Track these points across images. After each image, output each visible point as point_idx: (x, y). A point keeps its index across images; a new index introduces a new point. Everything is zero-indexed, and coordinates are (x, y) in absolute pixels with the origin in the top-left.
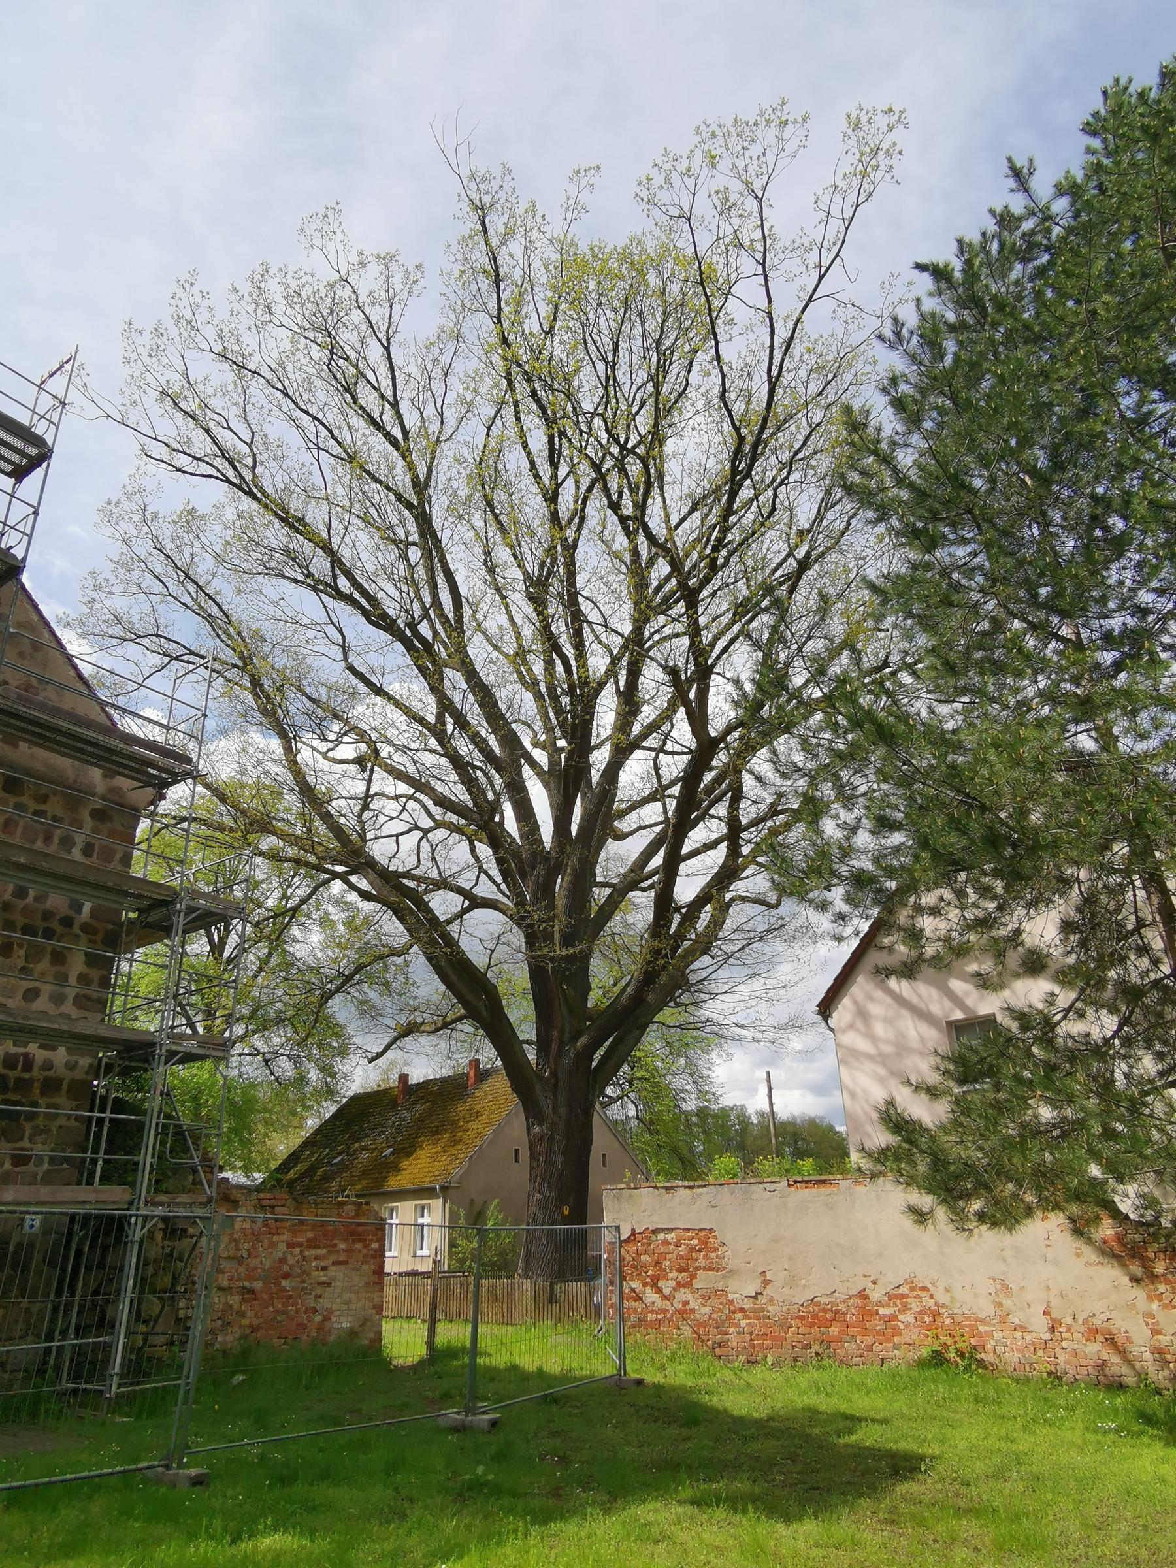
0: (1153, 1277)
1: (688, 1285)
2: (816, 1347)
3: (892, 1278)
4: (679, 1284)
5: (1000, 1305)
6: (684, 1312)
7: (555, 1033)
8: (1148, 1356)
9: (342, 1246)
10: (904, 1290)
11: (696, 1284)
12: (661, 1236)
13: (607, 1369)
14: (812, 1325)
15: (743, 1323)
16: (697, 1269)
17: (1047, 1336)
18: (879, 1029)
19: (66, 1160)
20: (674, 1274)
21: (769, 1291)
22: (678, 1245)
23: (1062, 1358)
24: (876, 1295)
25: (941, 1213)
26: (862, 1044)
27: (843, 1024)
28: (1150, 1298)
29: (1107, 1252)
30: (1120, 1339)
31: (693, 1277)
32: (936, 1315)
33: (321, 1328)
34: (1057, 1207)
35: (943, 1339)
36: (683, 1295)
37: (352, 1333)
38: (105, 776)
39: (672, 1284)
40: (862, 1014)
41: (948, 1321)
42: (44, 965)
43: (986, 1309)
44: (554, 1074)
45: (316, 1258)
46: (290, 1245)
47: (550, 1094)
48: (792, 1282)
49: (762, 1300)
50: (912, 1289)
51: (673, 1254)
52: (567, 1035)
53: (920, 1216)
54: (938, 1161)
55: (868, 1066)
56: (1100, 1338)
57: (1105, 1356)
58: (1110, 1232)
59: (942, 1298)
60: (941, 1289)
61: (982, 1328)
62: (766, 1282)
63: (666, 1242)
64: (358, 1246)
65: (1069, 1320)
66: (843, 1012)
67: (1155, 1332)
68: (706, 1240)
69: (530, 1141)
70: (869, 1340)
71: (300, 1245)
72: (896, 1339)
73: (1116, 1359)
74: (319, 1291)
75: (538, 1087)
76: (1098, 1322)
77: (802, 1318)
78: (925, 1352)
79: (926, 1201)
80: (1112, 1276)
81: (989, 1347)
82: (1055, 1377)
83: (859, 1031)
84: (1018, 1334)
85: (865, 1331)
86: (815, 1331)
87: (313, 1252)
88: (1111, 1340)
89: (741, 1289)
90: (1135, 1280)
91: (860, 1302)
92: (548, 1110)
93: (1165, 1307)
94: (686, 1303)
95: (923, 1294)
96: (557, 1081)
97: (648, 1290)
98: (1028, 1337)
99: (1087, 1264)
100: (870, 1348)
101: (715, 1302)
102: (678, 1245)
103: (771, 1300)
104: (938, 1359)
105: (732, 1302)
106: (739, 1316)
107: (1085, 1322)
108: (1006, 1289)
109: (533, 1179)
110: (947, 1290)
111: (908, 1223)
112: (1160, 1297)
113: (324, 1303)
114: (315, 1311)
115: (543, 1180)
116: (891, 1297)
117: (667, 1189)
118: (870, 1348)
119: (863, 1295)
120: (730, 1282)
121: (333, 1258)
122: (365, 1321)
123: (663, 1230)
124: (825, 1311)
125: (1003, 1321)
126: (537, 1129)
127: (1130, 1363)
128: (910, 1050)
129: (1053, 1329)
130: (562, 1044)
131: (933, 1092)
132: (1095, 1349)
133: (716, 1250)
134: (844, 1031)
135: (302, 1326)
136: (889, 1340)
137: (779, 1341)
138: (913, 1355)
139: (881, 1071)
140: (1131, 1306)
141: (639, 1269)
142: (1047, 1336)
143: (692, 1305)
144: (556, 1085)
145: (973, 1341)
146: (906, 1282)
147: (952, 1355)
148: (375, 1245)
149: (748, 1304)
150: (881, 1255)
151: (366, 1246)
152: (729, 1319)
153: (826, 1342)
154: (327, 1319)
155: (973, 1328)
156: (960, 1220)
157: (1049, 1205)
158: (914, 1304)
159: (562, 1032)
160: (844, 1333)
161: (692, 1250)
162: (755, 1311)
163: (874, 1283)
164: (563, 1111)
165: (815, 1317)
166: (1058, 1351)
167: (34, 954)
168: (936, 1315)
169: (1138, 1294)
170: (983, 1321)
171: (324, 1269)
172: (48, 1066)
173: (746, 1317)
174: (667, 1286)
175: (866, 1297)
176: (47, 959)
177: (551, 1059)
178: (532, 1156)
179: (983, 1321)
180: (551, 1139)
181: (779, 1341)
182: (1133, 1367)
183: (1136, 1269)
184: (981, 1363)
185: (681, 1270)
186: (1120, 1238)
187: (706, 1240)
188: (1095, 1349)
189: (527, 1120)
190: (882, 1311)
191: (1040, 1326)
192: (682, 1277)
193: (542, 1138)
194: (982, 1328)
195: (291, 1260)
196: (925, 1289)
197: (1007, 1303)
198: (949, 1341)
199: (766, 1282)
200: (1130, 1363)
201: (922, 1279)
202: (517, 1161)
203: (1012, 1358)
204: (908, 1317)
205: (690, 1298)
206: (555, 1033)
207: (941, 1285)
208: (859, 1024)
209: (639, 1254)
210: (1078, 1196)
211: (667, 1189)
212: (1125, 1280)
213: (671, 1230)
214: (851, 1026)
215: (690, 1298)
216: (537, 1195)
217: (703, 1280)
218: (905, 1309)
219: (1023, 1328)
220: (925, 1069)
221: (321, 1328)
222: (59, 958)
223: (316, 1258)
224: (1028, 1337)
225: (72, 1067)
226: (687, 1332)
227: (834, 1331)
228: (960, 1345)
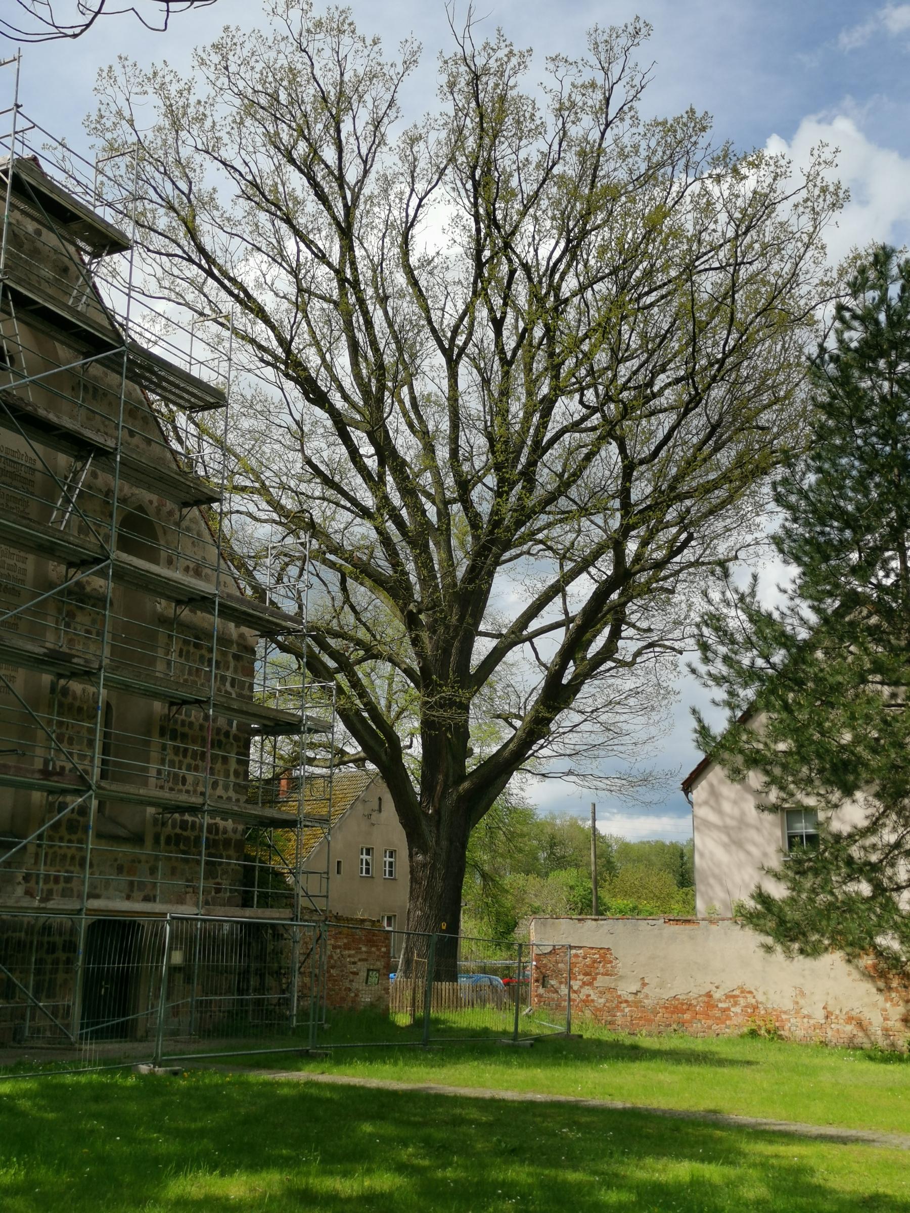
0: (890, 989)
1: (590, 984)
2: (674, 1026)
3: (730, 983)
4: (584, 984)
5: (797, 1003)
6: (587, 1001)
7: (441, 777)
8: (879, 1032)
9: (364, 949)
10: (737, 993)
11: (596, 984)
12: (573, 952)
13: (560, 1028)
14: (673, 1013)
15: (627, 1010)
16: (598, 974)
17: (823, 1021)
18: (727, 807)
19: (236, 890)
20: (581, 977)
21: (646, 990)
22: (585, 958)
23: (830, 1033)
24: (717, 995)
25: (779, 948)
26: (712, 817)
27: (700, 801)
28: (886, 1000)
29: (867, 975)
30: (865, 1023)
31: (594, 979)
32: (755, 1008)
33: (353, 1001)
34: (841, 948)
35: (758, 1022)
36: (587, 990)
37: (372, 1005)
38: (236, 626)
39: (579, 983)
40: (714, 792)
41: (763, 1012)
42: (219, 766)
43: (788, 1005)
44: (437, 812)
45: (349, 956)
46: (335, 947)
47: (434, 829)
48: (661, 985)
49: (640, 996)
50: (742, 992)
51: (581, 964)
52: (451, 779)
53: (769, 949)
54: (782, 922)
55: (716, 834)
56: (854, 1022)
57: (855, 1032)
58: (870, 962)
59: (761, 998)
60: (761, 992)
61: (784, 1017)
62: (644, 985)
63: (576, 956)
64: (373, 949)
65: (837, 1012)
66: (699, 792)
67: (886, 1019)
68: (605, 955)
69: (411, 867)
70: (710, 1022)
71: (339, 947)
72: (728, 1022)
73: (861, 1034)
74: (351, 976)
75: (424, 822)
76: (854, 1013)
77: (666, 1008)
78: (745, 1030)
79: (770, 940)
80: (868, 987)
81: (786, 1027)
82: (824, 1044)
83: (712, 807)
84: (806, 1020)
85: (708, 1017)
86: (675, 1016)
87: (346, 952)
88: (860, 1024)
89: (626, 989)
90: (880, 990)
91: (706, 999)
92: (432, 842)
93: (894, 1005)
94: (588, 996)
95: (748, 995)
96: (440, 818)
97: (563, 986)
98: (812, 1022)
99: (854, 980)
100: (710, 1027)
101: (608, 996)
102: (585, 958)
103: (647, 996)
104: (754, 1034)
105: (620, 996)
106: (624, 1005)
107: (847, 1013)
108: (802, 994)
109: (413, 896)
110: (764, 993)
111: (761, 952)
112: (892, 1000)
113: (355, 985)
114: (350, 990)
115: (425, 900)
116: (728, 997)
117: (579, 920)
118: (710, 1027)
119: (709, 995)
120: (619, 983)
121: (359, 957)
122: (380, 998)
123: (575, 947)
124: (682, 1004)
125: (797, 1012)
126: (420, 857)
127: (868, 1036)
128: (748, 825)
129: (827, 1017)
130: (446, 787)
131: (777, 877)
132: (850, 1028)
133: (611, 962)
134: (700, 805)
135: (343, 999)
136: (724, 1023)
137: (650, 1021)
138: (737, 1032)
139: (725, 839)
140: (875, 1005)
141: (558, 973)
142: (823, 1021)
143: (592, 997)
144: (439, 822)
145: (777, 1024)
146: (738, 988)
147: (763, 1032)
148: (383, 949)
149: (631, 998)
150: (724, 971)
151: (379, 950)
152: (617, 1007)
153: (681, 1023)
154: (356, 995)
155: (778, 1016)
156: (788, 952)
157: (836, 944)
158: (742, 1002)
159: (446, 776)
160: (694, 1018)
161: (594, 961)
162: (635, 1002)
163: (717, 987)
164: (444, 843)
165: (675, 1007)
166: (829, 1030)
167: (214, 758)
168: (755, 1008)
169: (880, 998)
170: (785, 1012)
171: (354, 963)
172: (225, 831)
173: (629, 1006)
174: (576, 985)
175: (711, 996)
176: (220, 761)
177: (436, 799)
178: (414, 880)
179: (785, 1012)
180: (433, 867)
181: (650, 1021)
182: (869, 1038)
183: (881, 984)
184: (780, 1037)
185: (586, 974)
186: (875, 966)
187: (605, 955)
188: (850, 1028)
189: (410, 850)
190: (720, 1005)
191: (819, 1015)
192: (586, 979)
193: (424, 866)
194: (784, 1017)
195: (335, 957)
196: (750, 992)
197: (802, 1002)
198: (762, 1023)
199: (644, 985)
200: (868, 1036)
201: (749, 987)
202: (339, 872)
203: (800, 1033)
204: (737, 1009)
205: (591, 992)
206: (441, 777)
207: (761, 990)
208: (712, 802)
209: (557, 963)
210: (852, 944)
211: (579, 920)
212: (874, 990)
213: (580, 948)
214: (706, 803)
215: (591, 992)
216: (419, 913)
217: (601, 981)
218: (736, 1004)
219: (809, 1017)
220: (775, 862)
221: (353, 1001)
222: (225, 760)
223: (349, 956)
224: (812, 1022)
225: (235, 831)
226: (588, 1014)
227: (687, 1016)
228: (769, 1026)
